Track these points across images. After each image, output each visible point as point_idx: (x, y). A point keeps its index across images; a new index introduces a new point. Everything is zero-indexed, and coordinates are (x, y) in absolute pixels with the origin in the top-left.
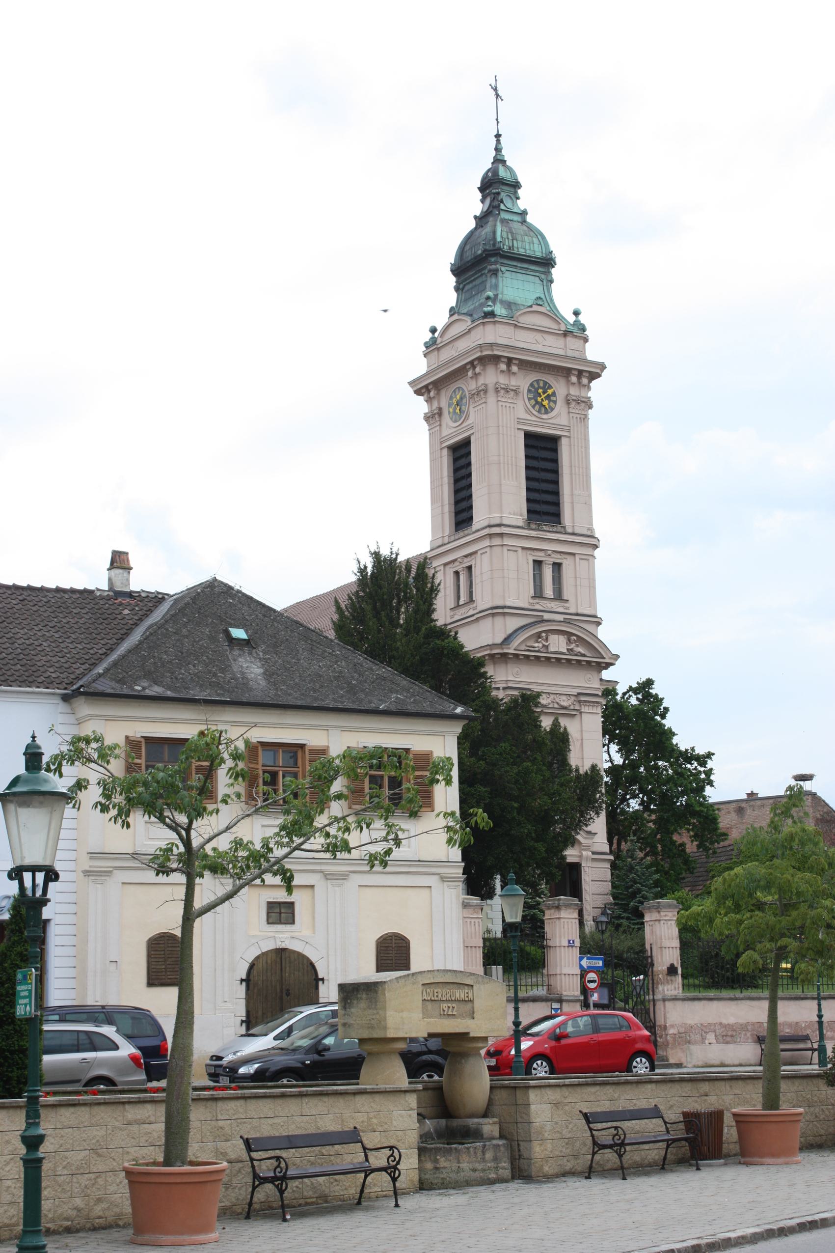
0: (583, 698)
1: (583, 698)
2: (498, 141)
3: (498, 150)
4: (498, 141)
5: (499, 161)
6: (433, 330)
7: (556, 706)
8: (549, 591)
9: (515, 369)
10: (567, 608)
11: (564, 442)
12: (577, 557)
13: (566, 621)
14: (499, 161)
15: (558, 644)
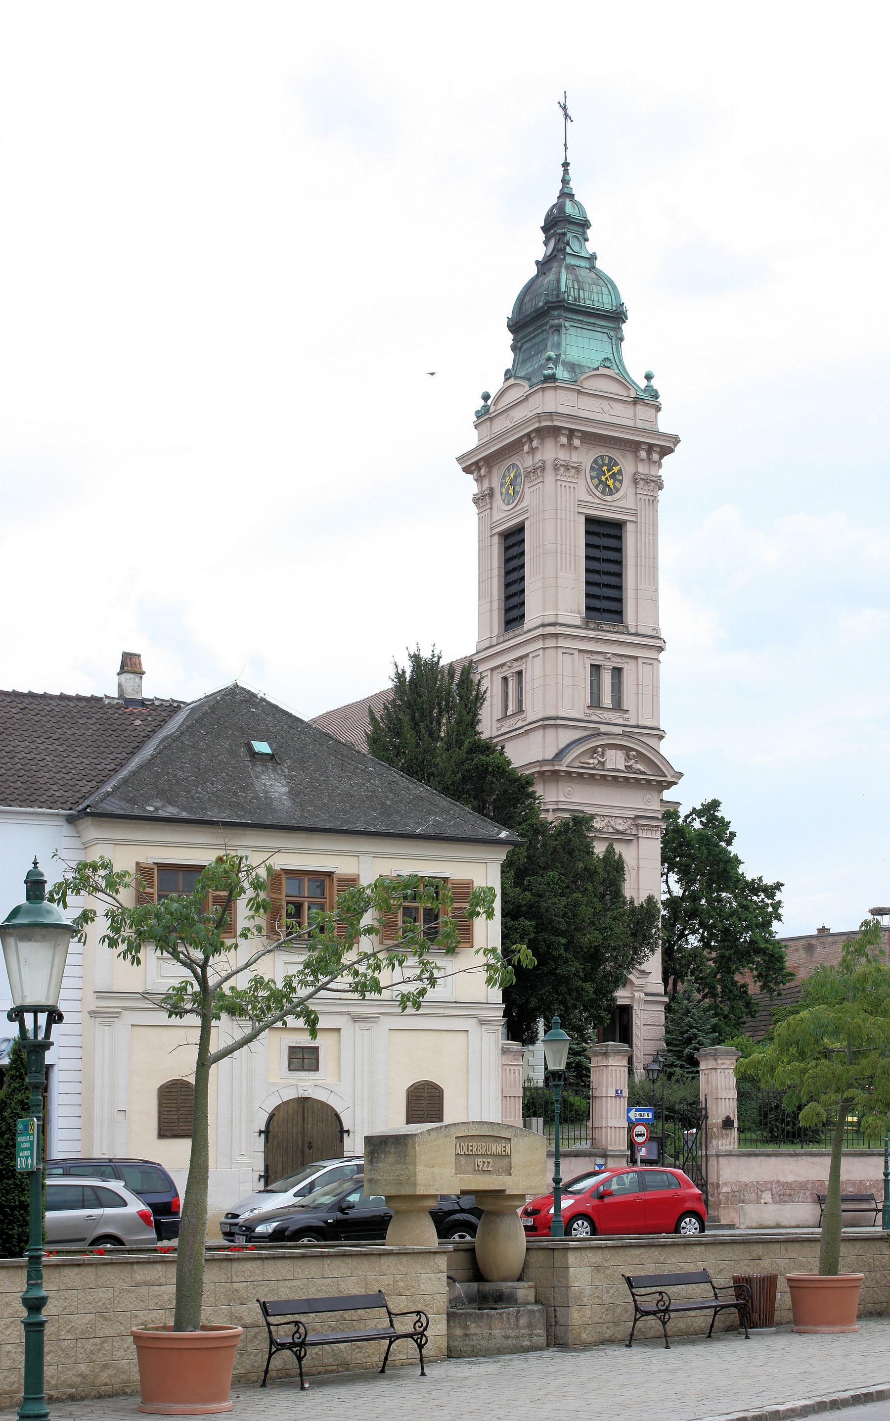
0: (641, 822)
1: (641, 822)
2: (566, 172)
3: (565, 181)
4: (566, 172)
5: (566, 194)
6: (486, 397)
7: (611, 830)
8: (607, 700)
9: (577, 442)
10: (627, 720)
11: (630, 527)
12: (640, 661)
13: (625, 735)
14: (566, 194)
15: (615, 761)
